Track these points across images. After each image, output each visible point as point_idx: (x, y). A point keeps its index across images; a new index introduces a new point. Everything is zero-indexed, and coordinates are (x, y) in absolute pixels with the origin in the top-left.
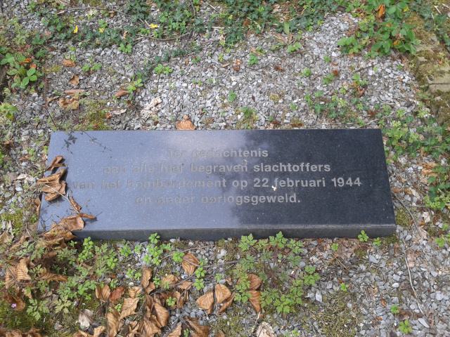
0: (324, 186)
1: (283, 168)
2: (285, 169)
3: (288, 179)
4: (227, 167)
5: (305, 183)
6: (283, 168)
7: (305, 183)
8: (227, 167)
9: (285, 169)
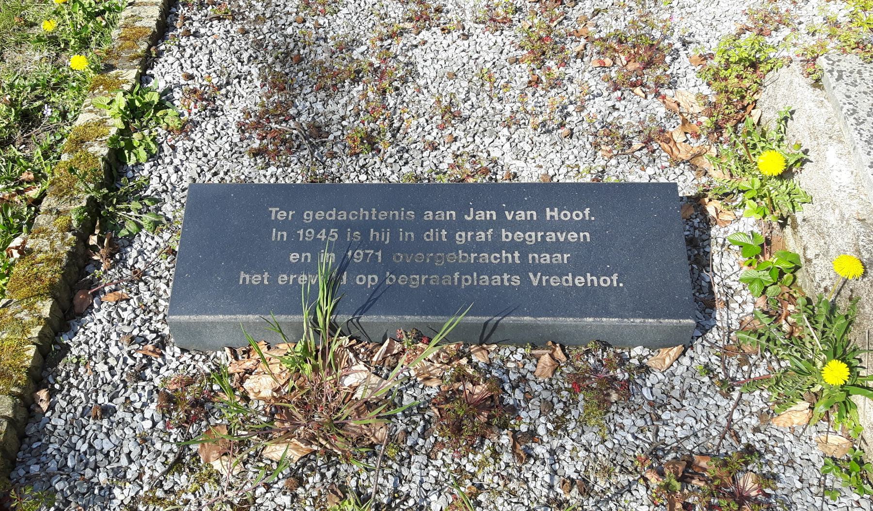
0: (588, 240)
1: (592, 281)
2: (378, 237)
3: (588, 275)
4: (559, 234)
5: (585, 236)
6: (592, 281)
7: (585, 236)
8: (559, 234)
9: (378, 237)
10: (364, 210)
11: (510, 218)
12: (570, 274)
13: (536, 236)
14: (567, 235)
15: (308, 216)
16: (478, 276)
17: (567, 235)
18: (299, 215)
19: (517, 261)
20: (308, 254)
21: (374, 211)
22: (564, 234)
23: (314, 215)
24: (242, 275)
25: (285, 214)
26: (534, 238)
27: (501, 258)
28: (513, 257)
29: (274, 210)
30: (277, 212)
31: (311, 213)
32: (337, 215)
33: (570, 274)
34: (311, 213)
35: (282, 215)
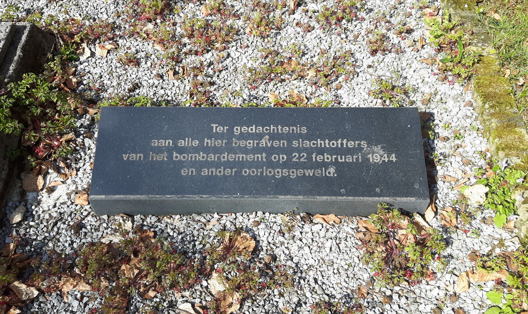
3: (325, 154)
10: (273, 126)
11: (125, 159)
12: (254, 126)
13: (253, 142)
14: (272, 142)
15: (237, 130)
16: (303, 141)
17: (272, 142)
18: (231, 131)
19: (264, 160)
20: (285, 142)
21: (280, 127)
22: (271, 142)
23: (241, 130)
24: (206, 140)
25: (222, 129)
26: (252, 144)
27: (317, 144)
28: (325, 143)
29: (214, 126)
30: (216, 127)
31: (239, 128)
32: (256, 129)
33: (254, 126)
34: (239, 128)
35: (220, 129)
